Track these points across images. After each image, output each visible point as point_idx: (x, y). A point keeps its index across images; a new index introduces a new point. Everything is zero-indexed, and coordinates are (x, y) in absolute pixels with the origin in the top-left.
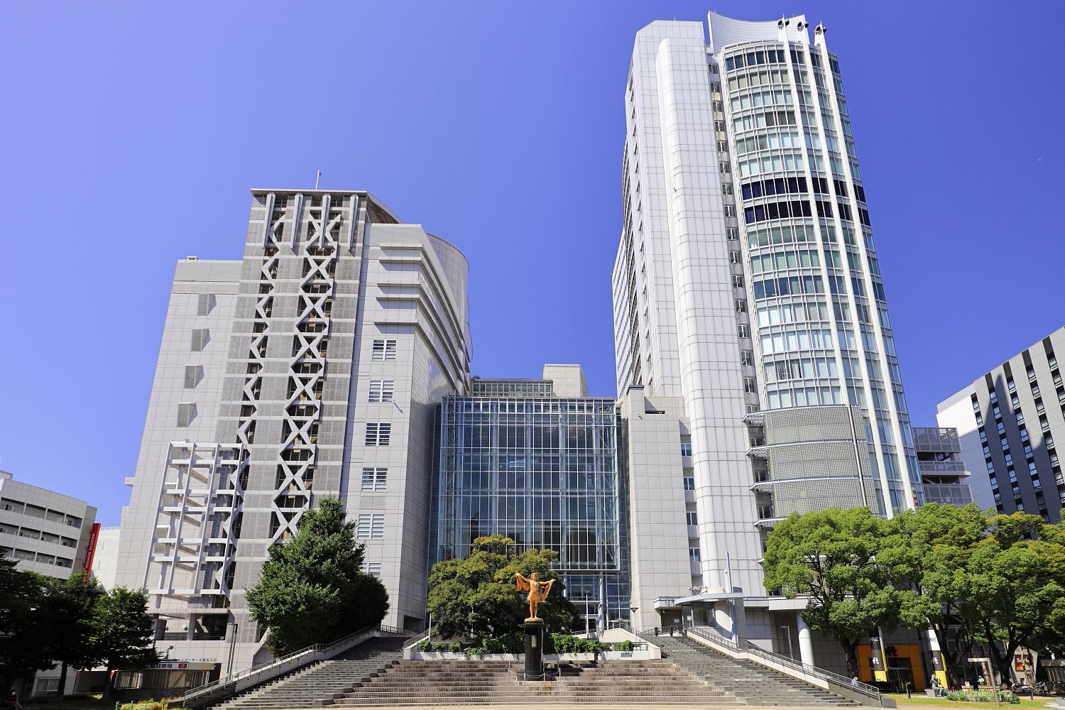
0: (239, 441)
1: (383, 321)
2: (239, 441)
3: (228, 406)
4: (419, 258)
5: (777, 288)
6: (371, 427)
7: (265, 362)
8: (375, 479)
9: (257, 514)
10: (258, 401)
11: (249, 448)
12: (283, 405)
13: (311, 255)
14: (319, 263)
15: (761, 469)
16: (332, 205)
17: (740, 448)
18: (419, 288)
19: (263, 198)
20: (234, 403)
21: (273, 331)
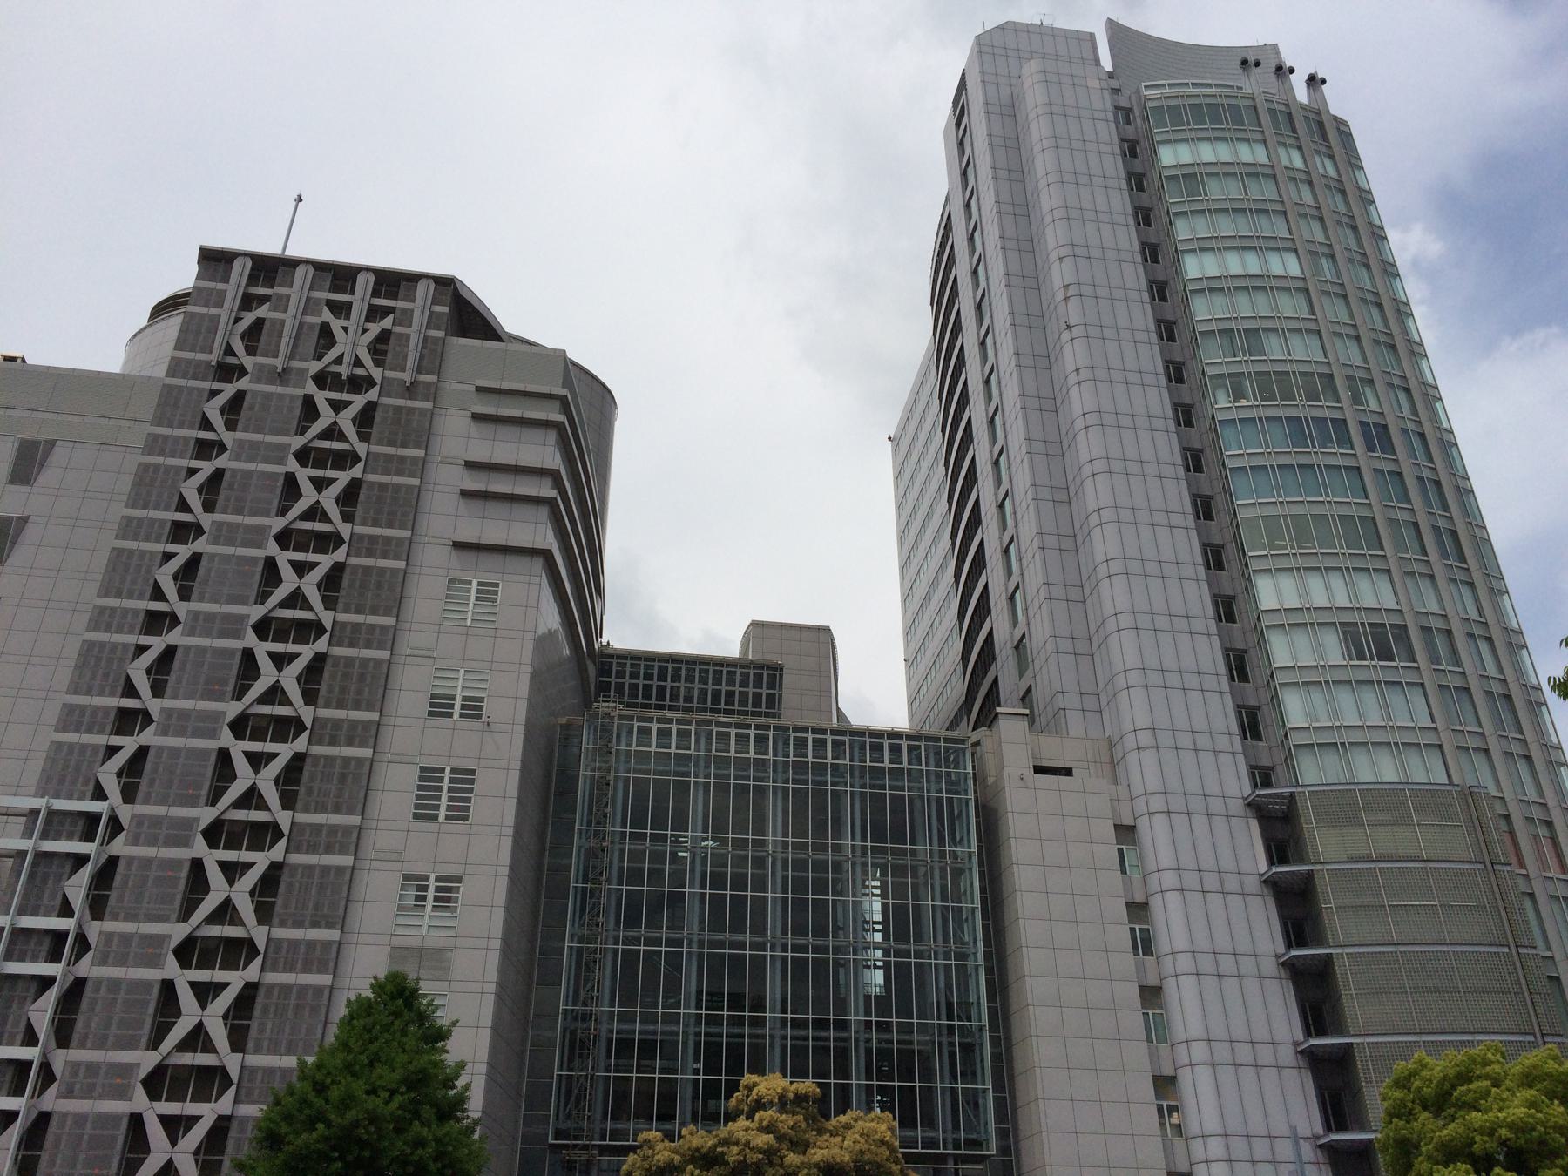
0: (100, 794)
1: (475, 541)
2: (100, 794)
3: (83, 708)
4: (548, 491)
5: (1287, 526)
6: (430, 776)
7: (163, 710)
8: (430, 902)
9: (124, 986)
10: (129, 806)
11: (125, 813)
12: (135, 1066)
13: (260, 639)
14: (337, 406)
15: (1297, 907)
16: (376, 294)
17: (1247, 866)
18: (554, 475)
19: (222, 266)
20: (99, 701)
21: (165, 733)
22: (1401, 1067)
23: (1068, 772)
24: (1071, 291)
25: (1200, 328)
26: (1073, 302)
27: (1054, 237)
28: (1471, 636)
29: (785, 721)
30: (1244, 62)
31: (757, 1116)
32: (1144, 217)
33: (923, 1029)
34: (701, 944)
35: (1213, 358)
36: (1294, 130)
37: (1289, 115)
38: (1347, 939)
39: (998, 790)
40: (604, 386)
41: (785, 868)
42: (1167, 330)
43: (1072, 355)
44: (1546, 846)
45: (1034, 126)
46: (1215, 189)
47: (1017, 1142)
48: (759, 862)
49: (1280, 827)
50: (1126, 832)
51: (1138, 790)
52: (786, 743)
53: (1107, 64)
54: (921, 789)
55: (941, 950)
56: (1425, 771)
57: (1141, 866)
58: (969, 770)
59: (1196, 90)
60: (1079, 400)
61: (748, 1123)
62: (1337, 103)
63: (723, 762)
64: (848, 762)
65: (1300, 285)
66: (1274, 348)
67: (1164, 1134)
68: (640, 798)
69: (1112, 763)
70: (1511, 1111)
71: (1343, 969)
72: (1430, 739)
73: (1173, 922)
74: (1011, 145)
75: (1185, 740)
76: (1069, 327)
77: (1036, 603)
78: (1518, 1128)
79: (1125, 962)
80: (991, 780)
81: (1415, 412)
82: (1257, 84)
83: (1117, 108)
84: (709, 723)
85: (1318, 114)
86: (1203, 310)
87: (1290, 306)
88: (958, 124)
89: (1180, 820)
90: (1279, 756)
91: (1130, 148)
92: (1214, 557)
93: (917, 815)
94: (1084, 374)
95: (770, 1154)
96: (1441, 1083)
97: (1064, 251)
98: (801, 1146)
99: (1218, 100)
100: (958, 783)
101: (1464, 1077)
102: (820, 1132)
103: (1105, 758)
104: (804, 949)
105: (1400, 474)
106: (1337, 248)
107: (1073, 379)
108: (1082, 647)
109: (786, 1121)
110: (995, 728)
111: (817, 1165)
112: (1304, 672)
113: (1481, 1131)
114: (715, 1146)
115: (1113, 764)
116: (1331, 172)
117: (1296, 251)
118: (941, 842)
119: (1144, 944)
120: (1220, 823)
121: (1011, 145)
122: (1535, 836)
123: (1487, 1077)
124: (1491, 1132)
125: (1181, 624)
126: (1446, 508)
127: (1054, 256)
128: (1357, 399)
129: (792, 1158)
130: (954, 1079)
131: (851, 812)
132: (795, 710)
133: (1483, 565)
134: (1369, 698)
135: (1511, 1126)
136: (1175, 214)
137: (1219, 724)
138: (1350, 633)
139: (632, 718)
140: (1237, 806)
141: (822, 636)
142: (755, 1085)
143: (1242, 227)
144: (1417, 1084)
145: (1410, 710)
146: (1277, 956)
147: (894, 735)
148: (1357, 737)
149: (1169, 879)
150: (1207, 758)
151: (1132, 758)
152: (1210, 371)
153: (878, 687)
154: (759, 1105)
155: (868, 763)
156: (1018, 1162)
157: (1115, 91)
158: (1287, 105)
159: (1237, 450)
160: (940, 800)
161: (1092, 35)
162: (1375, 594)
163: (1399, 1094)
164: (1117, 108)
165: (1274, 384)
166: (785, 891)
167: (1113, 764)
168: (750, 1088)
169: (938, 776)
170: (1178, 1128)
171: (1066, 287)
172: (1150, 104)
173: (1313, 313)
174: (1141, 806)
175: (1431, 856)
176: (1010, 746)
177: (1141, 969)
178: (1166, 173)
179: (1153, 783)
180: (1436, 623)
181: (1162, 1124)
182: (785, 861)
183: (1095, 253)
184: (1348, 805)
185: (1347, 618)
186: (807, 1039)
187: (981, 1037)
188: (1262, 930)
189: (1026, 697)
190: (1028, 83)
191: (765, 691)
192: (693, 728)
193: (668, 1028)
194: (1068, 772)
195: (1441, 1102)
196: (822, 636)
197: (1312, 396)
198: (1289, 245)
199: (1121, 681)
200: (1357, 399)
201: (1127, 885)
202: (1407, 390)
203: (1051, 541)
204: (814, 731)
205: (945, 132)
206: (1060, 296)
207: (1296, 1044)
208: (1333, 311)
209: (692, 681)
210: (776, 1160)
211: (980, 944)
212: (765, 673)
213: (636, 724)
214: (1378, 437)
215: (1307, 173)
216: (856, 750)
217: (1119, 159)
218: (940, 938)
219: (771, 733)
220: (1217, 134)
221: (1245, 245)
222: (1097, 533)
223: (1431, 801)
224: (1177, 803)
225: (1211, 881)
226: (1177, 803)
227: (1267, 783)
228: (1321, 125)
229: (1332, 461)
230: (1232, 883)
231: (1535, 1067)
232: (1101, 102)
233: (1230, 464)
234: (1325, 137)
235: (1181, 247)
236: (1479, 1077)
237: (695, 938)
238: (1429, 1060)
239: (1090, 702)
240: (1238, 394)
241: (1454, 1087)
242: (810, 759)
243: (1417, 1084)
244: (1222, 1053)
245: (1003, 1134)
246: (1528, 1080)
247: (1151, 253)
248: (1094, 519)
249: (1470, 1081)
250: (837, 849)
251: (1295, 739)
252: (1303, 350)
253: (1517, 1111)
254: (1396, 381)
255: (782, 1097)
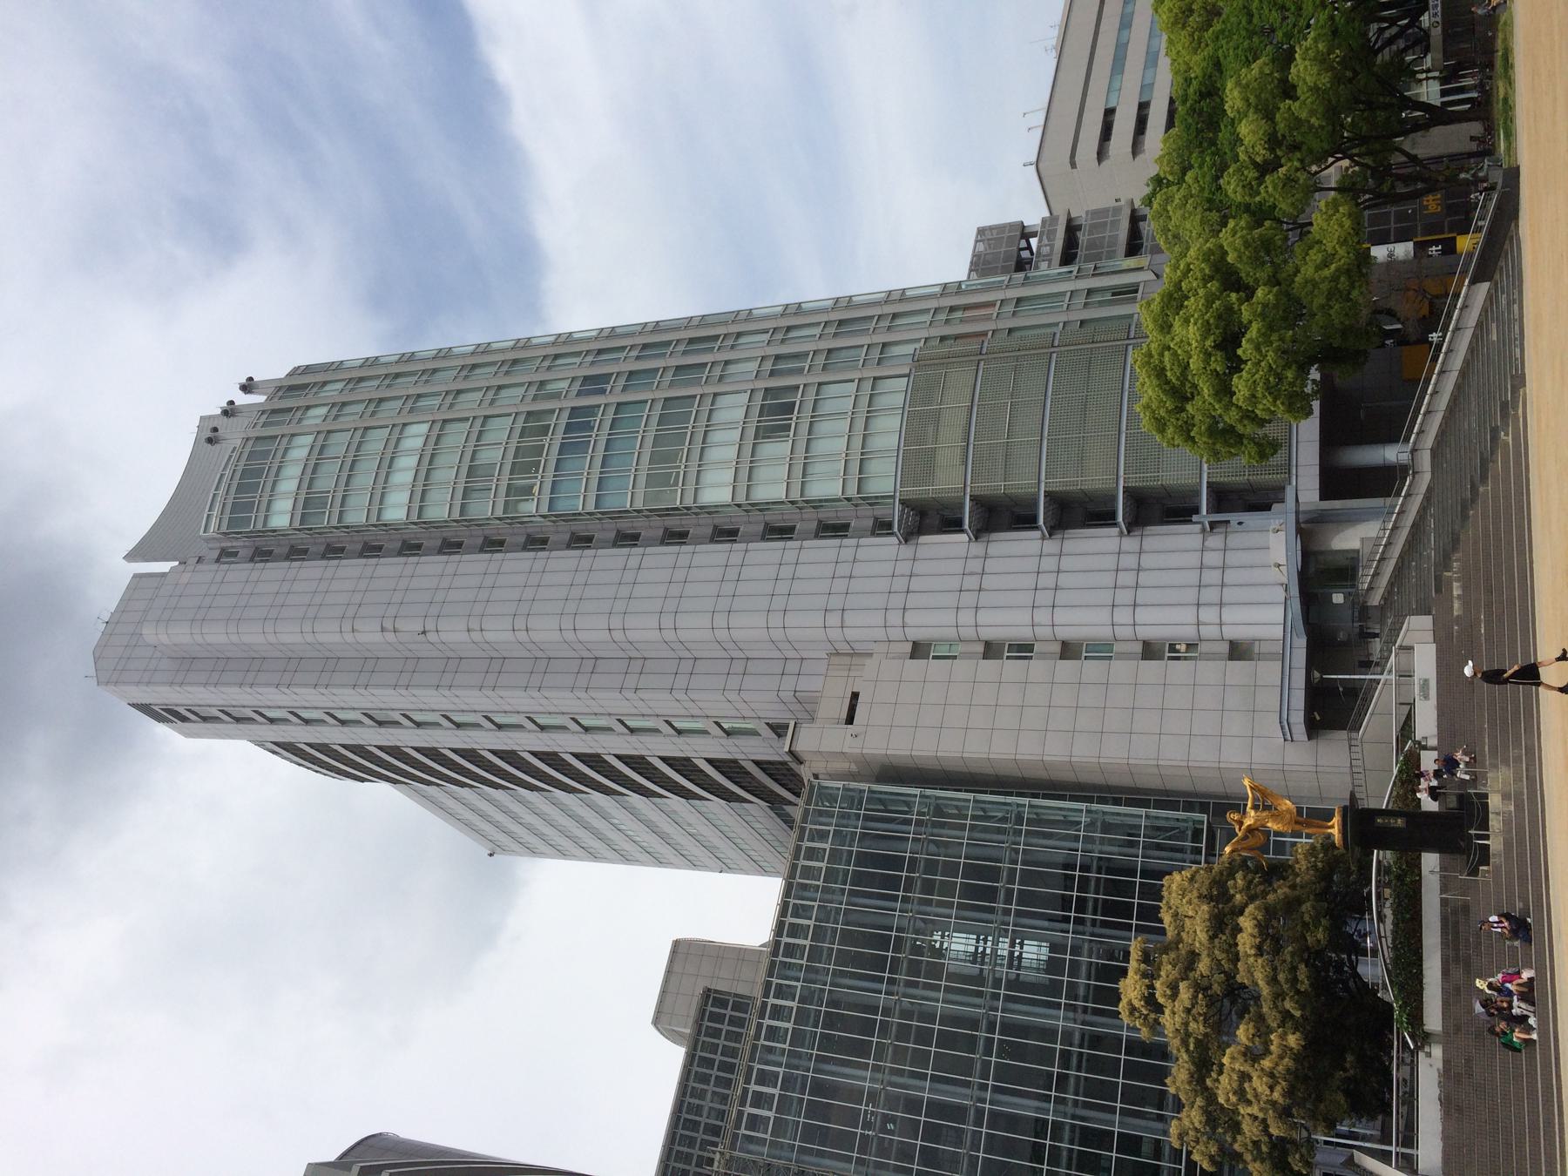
15: (1000, 515)
22: (1146, 423)
23: (855, 696)
24: (388, 624)
25: (456, 515)
26: (400, 625)
27: (329, 635)
28: (783, 341)
29: (758, 992)
30: (210, 441)
31: (1161, 1000)
32: (333, 551)
33: (1076, 950)
34: (984, 1087)
35: (485, 507)
36: (289, 410)
37: (274, 412)
38: (1033, 478)
39: (863, 761)
40: (359, 1143)
41: (900, 1073)
42: (451, 547)
43: (453, 633)
44: (968, 314)
45: (210, 639)
46: (325, 482)
47: (1196, 795)
48: (892, 1101)
49: (927, 518)
50: (919, 650)
51: (880, 634)
52: (770, 1050)
53: (164, 567)
54: (838, 911)
55: (1012, 838)
56: (895, 393)
57: (951, 643)
58: (840, 784)
59: (223, 486)
60: (498, 633)
61: (1167, 1011)
62: (275, 369)
63: (798, 1039)
64: (799, 984)
65: (437, 426)
66: (490, 456)
67: (1194, 658)
68: (858, 960)
69: (853, 655)
70: (1191, 336)
71: (1060, 484)
72: (868, 385)
73: (1007, 623)
74: (220, 665)
75: (840, 585)
76: (424, 632)
77: (689, 705)
78: (1206, 330)
79: (1037, 668)
80: (854, 768)
81: (578, 354)
82: (234, 435)
83: (218, 561)
84: (754, 1047)
85: (280, 388)
86: (439, 509)
87: (456, 436)
88: (184, 719)
89: (913, 600)
90: (866, 510)
91: (262, 555)
92: (675, 537)
93: (868, 920)
94: (475, 625)
95: (1200, 988)
96: (1164, 391)
97: (347, 627)
98: (1193, 957)
99: (240, 468)
100: (852, 799)
101: (1160, 372)
102: (1179, 940)
103: (847, 660)
104: (1009, 892)
105: (631, 373)
106: (411, 392)
107: (476, 636)
108: (738, 667)
109: (1167, 971)
110: (805, 757)
111: (1212, 938)
112: (793, 475)
113: (1207, 362)
114: (1187, 1050)
115: (854, 654)
116: (323, 411)
117: (405, 425)
118: (908, 822)
119: (1023, 650)
120: (920, 567)
121: (220, 665)
122: (962, 321)
123: (1161, 355)
124: (1208, 355)
125: (732, 574)
126: (668, 343)
127: (349, 638)
128: (556, 396)
129: (1203, 966)
130: (1112, 1110)
131: (852, 990)
132: (749, 984)
133: (721, 323)
134: (824, 427)
135: (1204, 338)
136: (340, 521)
137: (831, 554)
138: (765, 433)
139: (735, 1136)
140: (907, 551)
141: (681, 950)
142: (1130, 1003)
143: (368, 467)
144: (1162, 412)
145: (840, 398)
146: (1043, 538)
147: (787, 892)
148: (857, 442)
149: (966, 617)
150: (859, 569)
151: (851, 634)
152: (499, 513)
153: (740, 907)
154: (1150, 1000)
155: (804, 962)
156: (1216, 797)
157: (200, 560)
158: (263, 412)
159: (579, 499)
160: (867, 818)
161: (136, 576)
162: (733, 409)
163: (1170, 431)
164: (218, 561)
165: (526, 461)
166: (923, 1077)
167: (854, 654)
168: (1133, 1010)
169: (843, 816)
170: (1191, 646)
171: (383, 630)
172: (224, 529)
173: (467, 419)
174: (896, 634)
175: (969, 398)
176: (824, 745)
177: (1044, 656)
178: (296, 524)
179: (878, 618)
180: (768, 366)
181: (1186, 658)
182: (909, 984)
183: (357, 598)
184: (916, 459)
185: (751, 432)
186: (1096, 900)
187: (1096, 812)
188: (1018, 550)
189: (779, 729)
190: (164, 639)
191: (715, 1072)
192: (757, 1066)
193: (1064, 1161)
194: (855, 696)
195: (1180, 394)
196: (681, 950)
197: (544, 430)
198: (397, 430)
199: (777, 634)
200: (556, 396)
201: (968, 656)
202: (557, 357)
203: (631, 681)
204: (766, 995)
205: (187, 735)
206: (390, 637)
207: (1121, 534)
208: (470, 404)
209: (697, 1124)
210: (1205, 983)
211: (1009, 799)
212: (709, 1008)
213: (743, 1131)
214: (594, 384)
215: (334, 405)
216: (806, 894)
217: (269, 565)
218: (1000, 837)
219: (775, 981)
220: (268, 489)
221: (387, 464)
222: (631, 635)
223: (924, 391)
224: (897, 601)
225: (971, 582)
226: (897, 601)
227: (889, 525)
228: (291, 388)
229: (607, 424)
230: (975, 565)
231: (1155, 321)
232: (208, 571)
233: (591, 507)
234: (304, 387)
235: (373, 520)
236: (1161, 362)
237: (977, 1093)
238: (1144, 400)
239: (792, 667)
240: (528, 491)
241: (1168, 382)
242: (823, 865)
243: (1162, 412)
244: (1125, 597)
245: (1189, 807)
246: (1166, 328)
247: (371, 550)
248: (618, 635)
249: (1164, 369)
250: (887, 1012)
251: (852, 491)
252: (499, 431)
253: (1193, 332)
254: (546, 364)
255: (1144, 975)
